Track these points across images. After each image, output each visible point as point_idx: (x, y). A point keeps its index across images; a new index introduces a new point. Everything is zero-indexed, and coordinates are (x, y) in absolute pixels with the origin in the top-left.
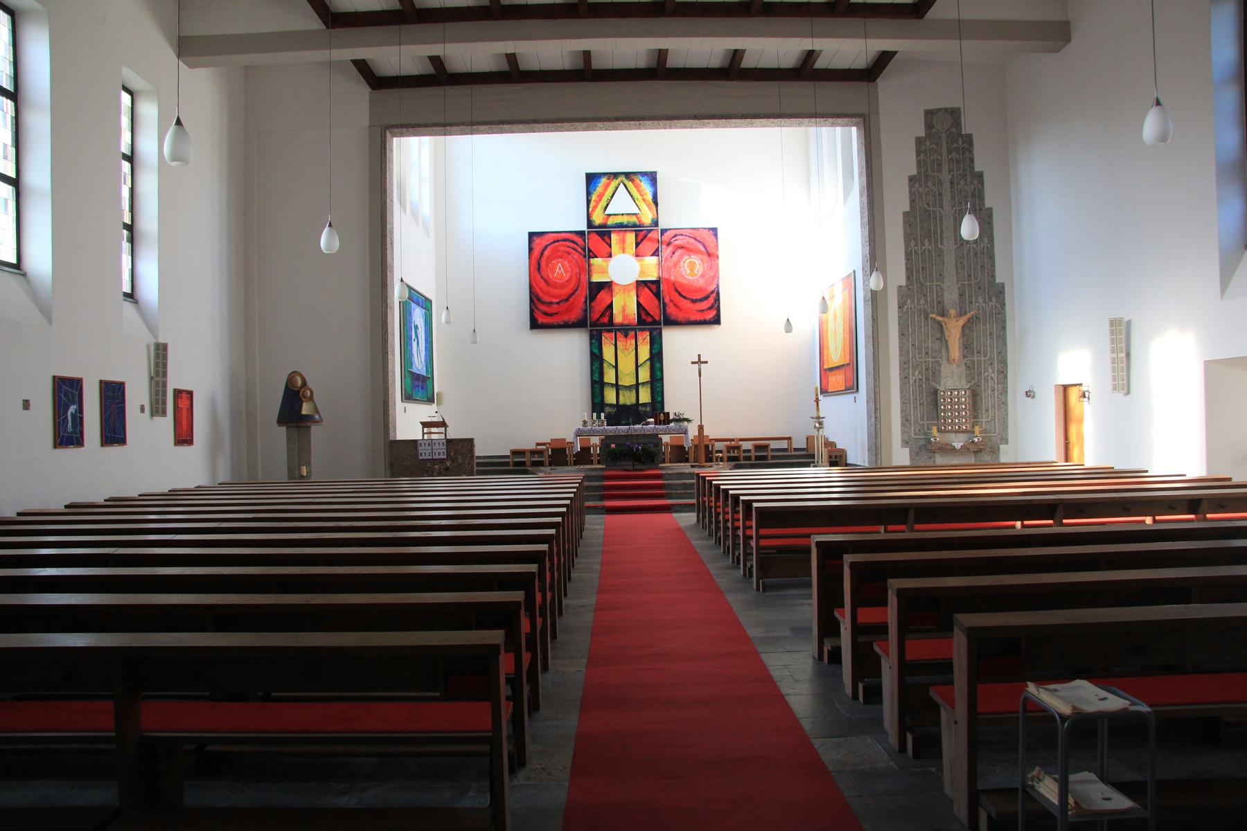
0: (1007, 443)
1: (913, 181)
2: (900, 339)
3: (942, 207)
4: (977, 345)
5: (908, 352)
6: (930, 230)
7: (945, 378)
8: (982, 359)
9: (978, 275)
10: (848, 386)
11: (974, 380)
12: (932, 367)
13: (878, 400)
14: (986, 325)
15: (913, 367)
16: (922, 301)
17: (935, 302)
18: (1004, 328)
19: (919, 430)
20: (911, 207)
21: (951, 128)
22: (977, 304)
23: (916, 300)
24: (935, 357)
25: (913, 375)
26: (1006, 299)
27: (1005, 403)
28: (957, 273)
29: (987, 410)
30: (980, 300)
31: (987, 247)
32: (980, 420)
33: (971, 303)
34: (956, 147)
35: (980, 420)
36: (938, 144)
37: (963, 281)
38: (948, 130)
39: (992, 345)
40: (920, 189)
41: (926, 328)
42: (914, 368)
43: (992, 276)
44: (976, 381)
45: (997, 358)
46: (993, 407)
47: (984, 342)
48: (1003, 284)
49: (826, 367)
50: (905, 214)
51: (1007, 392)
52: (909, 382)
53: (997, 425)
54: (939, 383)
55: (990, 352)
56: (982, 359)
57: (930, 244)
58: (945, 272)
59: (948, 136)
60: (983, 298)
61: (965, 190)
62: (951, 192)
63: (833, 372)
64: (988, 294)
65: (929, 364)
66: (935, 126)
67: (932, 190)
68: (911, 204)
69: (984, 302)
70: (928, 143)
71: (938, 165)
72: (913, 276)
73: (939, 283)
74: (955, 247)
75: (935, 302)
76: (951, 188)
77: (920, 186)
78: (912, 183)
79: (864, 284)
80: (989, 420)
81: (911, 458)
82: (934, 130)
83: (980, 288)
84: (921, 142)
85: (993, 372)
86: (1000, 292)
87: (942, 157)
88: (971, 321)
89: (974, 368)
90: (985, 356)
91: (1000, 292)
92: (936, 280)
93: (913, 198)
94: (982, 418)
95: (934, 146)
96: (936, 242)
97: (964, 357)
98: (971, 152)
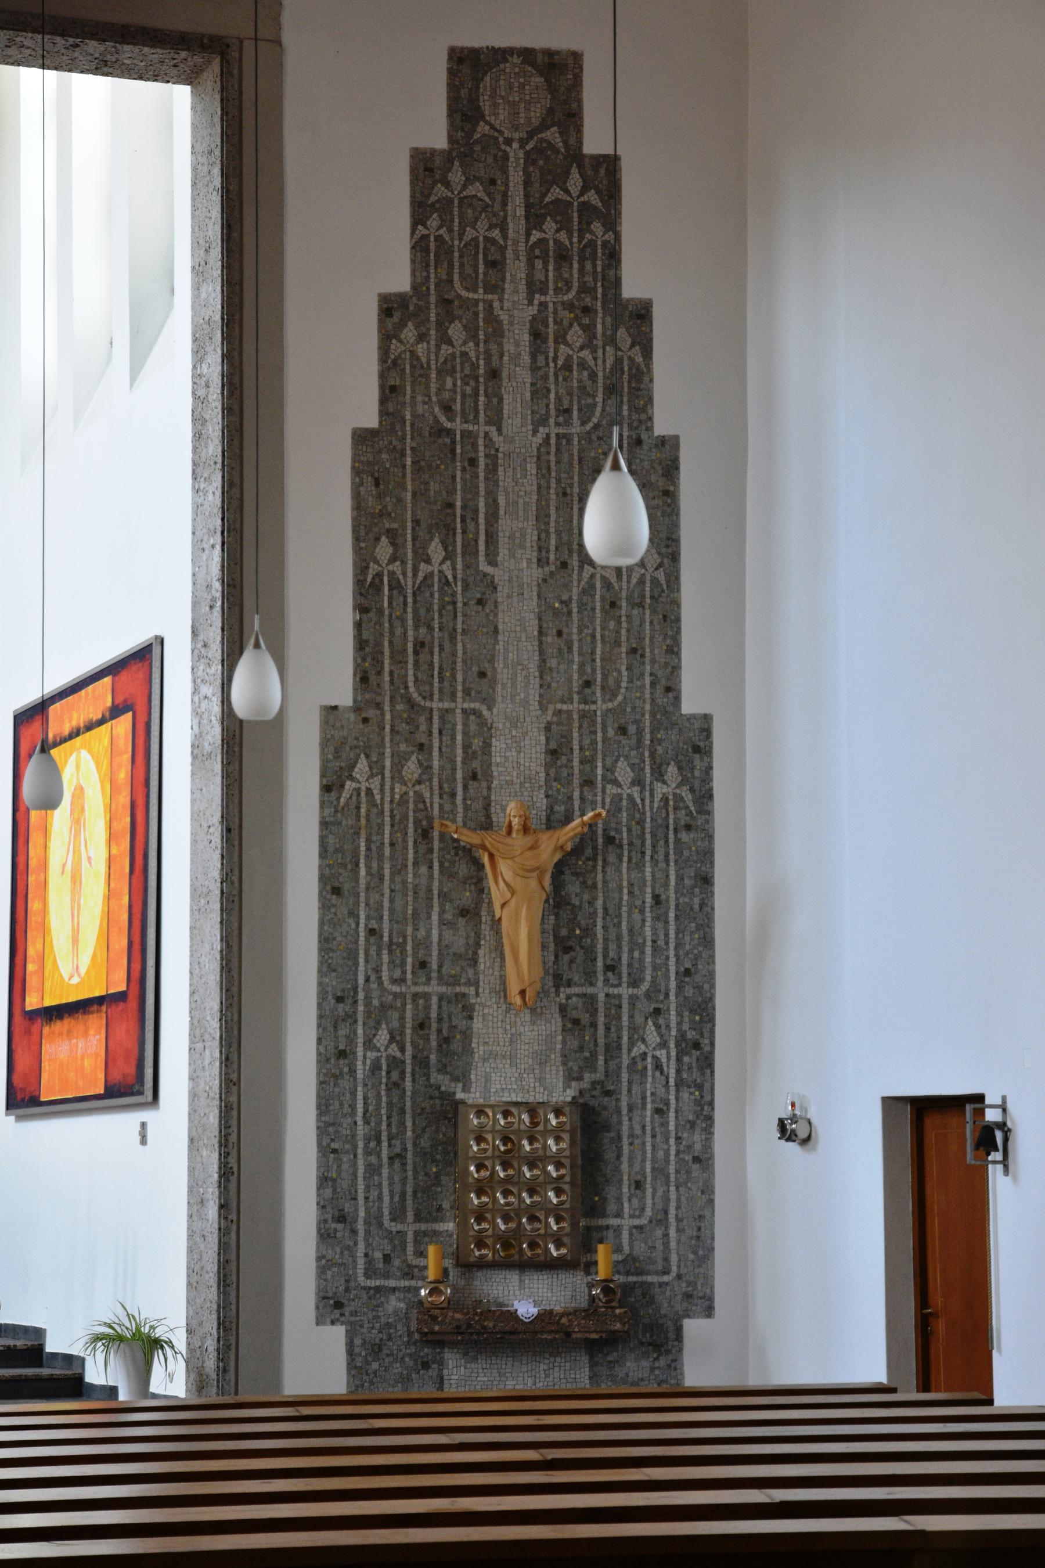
0: (709, 1311)
1: (397, 317)
2: (325, 906)
3: (496, 420)
4: (606, 940)
5: (353, 955)
6: (451, 505)
7: (485, 1060)
8: (625, 991)
9: (618, 682)
10: (117, 1076)
11: (593, 1069)
12: (440, 1020)
13: (233, 1138)
14: (640, 866)
15: (368, 1014)
16: (412, 768)
17: (459, 775)
18: (706, 881)
19: (387, 1258)
20: (383, 413)
21: (543, 126)
22: (611, 790)
23: (388, 763)
24: (454, 981)
25: (369, 1044)
26: (717, 774)
27: (704, 1160)
28: (543, 669)
29: (638, 1185)
30: (624, 772)
31: (655, 581)
32: (613, 1222)
33: (588, 782)
34: (557, 201)
35: (613, 1222)
36: (493, 182)
37: (563, 702)
38: (531, 134)
39: (661, 943)
40: (421, 349)
41: (423, 870)
42: (377, 1017)
43: (668, 689)
44: (599, 1076)
45: (680, 988)
46: (660, 1172)
47: (631, 931)
48: (707, 718)
49: (32, 1002)
50: (362, 438)
51: (710, 1119)
52: (352, 1072)
53: (673, 1244)
54: (463, 1078)
55: (655, 968)
56: (625, 991)
57: (449, 556)
58: (499, 665)
59: (529, 159)
60: (632, 766)
61: (583, 365)
62: (534, 369)
63: (58, 1026)
64: (652, 756)
65: (427, 1007)
66: (487, 110)
67: (464, 354)
68: (383, 401)
69: (638, 782)
70: (456, 177)
71: (492, 264)
72: (379, 673)
73: (476, 705)
74: (537, 573)
75: (459, 775)
76: (534, 357)
77: (422, 337)
78: (389, 324)
79: (195, 691)
80: (644, 1221)
81: (351, 1365)
82: (482, 128)
83: (623, 730)
84: (430, 170)
85: (664, 1044)
86: (697, 749)
87: (505, 237)
88: (588, 852)
89: (594, 1025)
90: (634, 983)
91: (697, 749)
92: (467, 692)
93: (394, 380)
94: (619, 1215)
95: (476, 189)
96: (470, 549)
97: (559, 980)
98: (612, 222)
